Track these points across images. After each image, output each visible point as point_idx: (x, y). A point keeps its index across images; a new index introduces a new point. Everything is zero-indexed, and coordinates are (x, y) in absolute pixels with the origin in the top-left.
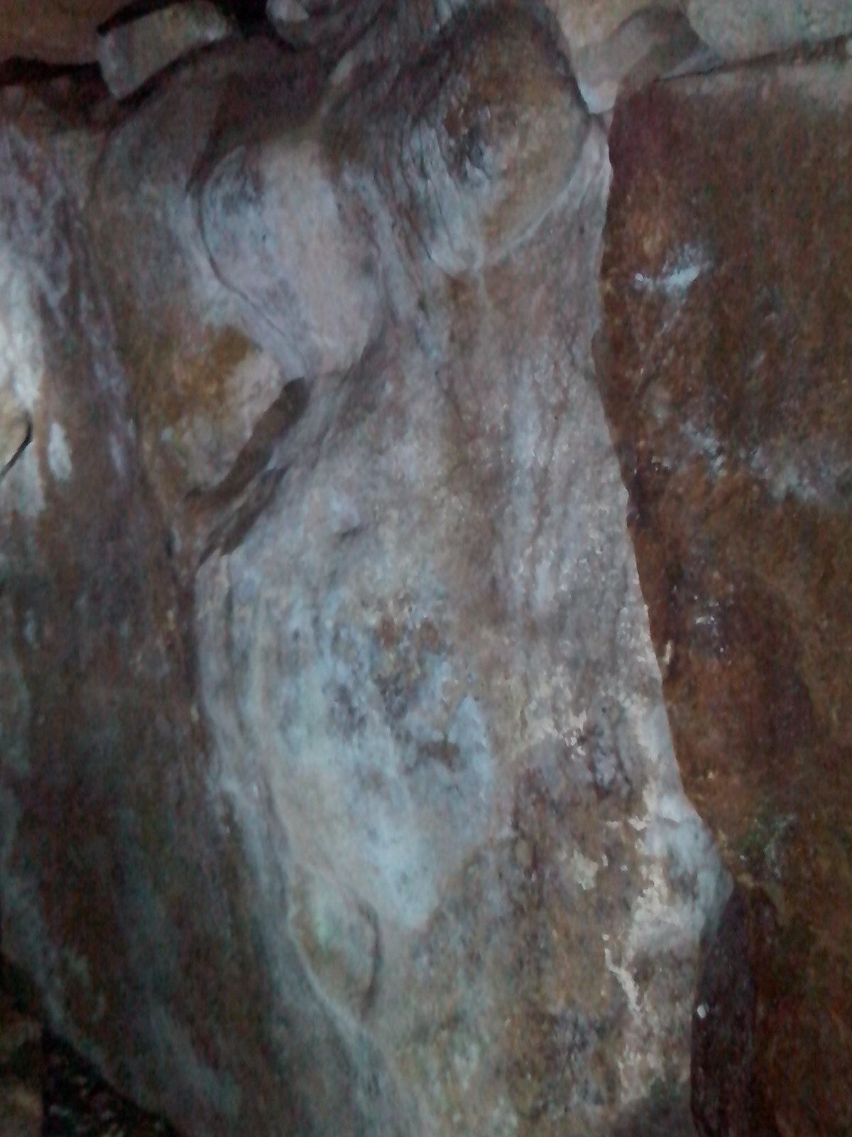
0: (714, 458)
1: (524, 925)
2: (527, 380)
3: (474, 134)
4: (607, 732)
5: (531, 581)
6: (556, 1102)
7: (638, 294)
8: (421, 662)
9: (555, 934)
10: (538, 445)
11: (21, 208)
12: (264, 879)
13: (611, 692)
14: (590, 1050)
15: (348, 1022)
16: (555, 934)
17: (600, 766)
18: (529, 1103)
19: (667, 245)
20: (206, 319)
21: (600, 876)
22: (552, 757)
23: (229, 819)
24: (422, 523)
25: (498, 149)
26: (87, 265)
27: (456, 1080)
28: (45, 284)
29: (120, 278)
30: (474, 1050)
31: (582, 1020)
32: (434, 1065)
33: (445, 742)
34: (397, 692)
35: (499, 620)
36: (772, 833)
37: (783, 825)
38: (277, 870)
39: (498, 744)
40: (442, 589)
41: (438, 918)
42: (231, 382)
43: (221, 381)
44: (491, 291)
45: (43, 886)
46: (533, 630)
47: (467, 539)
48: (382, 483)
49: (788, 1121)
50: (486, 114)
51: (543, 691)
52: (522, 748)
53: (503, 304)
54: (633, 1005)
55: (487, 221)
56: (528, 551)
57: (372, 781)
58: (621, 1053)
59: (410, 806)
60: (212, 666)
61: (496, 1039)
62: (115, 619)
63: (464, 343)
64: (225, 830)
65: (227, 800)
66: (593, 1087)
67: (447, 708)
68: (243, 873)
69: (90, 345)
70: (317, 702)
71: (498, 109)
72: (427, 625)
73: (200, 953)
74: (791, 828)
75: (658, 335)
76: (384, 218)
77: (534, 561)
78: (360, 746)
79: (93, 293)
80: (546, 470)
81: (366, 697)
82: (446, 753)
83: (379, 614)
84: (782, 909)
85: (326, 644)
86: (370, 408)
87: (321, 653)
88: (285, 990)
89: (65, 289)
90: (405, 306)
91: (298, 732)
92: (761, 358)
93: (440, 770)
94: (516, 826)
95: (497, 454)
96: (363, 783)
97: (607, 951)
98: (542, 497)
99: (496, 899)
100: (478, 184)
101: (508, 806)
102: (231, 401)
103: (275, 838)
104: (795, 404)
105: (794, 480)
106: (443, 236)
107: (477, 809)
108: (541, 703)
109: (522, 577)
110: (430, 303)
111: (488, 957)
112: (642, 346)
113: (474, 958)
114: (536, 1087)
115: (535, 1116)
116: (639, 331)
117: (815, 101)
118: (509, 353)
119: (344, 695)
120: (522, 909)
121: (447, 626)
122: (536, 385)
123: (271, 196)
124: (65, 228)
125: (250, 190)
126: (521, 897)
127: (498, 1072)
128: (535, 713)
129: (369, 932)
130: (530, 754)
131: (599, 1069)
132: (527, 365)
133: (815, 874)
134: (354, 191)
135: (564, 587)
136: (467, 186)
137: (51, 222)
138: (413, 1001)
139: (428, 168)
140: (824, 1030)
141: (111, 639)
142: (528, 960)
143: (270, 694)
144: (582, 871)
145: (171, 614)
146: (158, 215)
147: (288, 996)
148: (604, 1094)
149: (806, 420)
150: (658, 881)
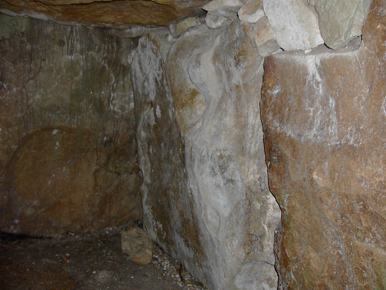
0: (278, 127)
1: (247, 216)
2: (251, 106)
3: (239, 61)
4: (263, 178)
5: (250, 148)
6: (252, 251)
7: (268, 94)
8: (227, 163)
9: (253, 218)
10: (253, 120)
11: (152, 59)
12: (198, 206)
13: (264, 170)
14: (258, 241)
15: (214, 235)
16: (253, 218)
17: (262, 185)
18: (247, 251)
19: (273, 85)
20: (189, 87)
21: (261, 207)
22: (253, 183)
23: (191, 194)
24: (229, 134)
25: (243, 64)
26: (166, 74)
27: (233, 246)
28: (157, 76)
29: (172, 77)
30: (237, 241)
31: (257, 235)
32: (229, 243)
33: (232, 179)
34: (223, 169)
35: (243, 155)
36: (285, 197)
37: (287, 196)
38: (200, 205)
39: (242, 180)
40: (232, 148)
41: (231, 214)
42: (194, 100)
43: (192, 100)
44: (244, 88)
45: (153, 208)
46: (250, 157)
47: (238, 138)
48: (222, 126)
49: (288, 251)
50: (241, 57)
51: (251, 170)
52: (247, 181)
53: (247, 91)
54: (267, 232)
55: (242, 76)
56: (250, 141)
57: (218, 186)
58: (264, 241)
59: (225, 191)
60: (188, 161)
61: (241, 238)
62: (169, 149)
63: (239, 98)
64: (190, 196)
65: (191, 189)
66: (259, 248)
67: (232, 172)
68: (194, 205)
69: (166, 90)
70: (208, 170)
71: (243, 57)
72: (229, 155)
73: (185, 223)
74: (288, 197)
75: (271, 102)
76: (224, 72)
77: (251, 143)
78: (216, 179)
79: (166, 80)
80: (254, 125)
81: (217, 169)
82: (232, 181)
83: (220, 153)
84: (287, 212)
85: (210, 158)
86: (220, 110)
87: (209, 160)
88: (202, 229)
89: (161, 78)
90: (228, 89)
91: (204, 176)
92: (288, 109)
93: (231, 184)
94: (246, 197)
95: (245, 121)
96: (216, 186)
97: (262, 221)
98: (253, 130)
99: (242, 211)
100: (240, 70)
101: (244, 192)
102: (194, 104)
103: (200, 197)
104: (292, 118)
105: (290, 133)
106: (234, 78)
107: (238, 193)
108: (251, 172)
109: (248, 146)
110: (232, 89)
111: (240, 222)
112: (268, 104)
113: (237, 222)
114: (248, 248)
115: (248, 253)
116: (268, 101)
117: (297, 62)
118: (248, 101)
119: (213, 169)
120: (247, 213)
121: (233, 156)
122: (253, 107)
123: (202, 66)
124: (161, 64)
125: (198, 65)
126: (247, 211)
127: (241, 245)
128: (250, 174)
129: (218, 217)
130: (249, 182)
131: (260, 244)
132: (251, 103)
133: (292, 205)
134: (218, 67)
135: (257, 149)
136: (238, 70)
137: (158, 63)
138: (226, 231)
139: (231, 65)
140: (294, 234)
141: (168, 153)
142: (248, 223)
143: (199, 168)
144: (258, 206)
145: (180, 149)
146: (180, 65)
147: (202, 231)
148: (261, 249)
149: (293, 122)
150: (271, 208)
